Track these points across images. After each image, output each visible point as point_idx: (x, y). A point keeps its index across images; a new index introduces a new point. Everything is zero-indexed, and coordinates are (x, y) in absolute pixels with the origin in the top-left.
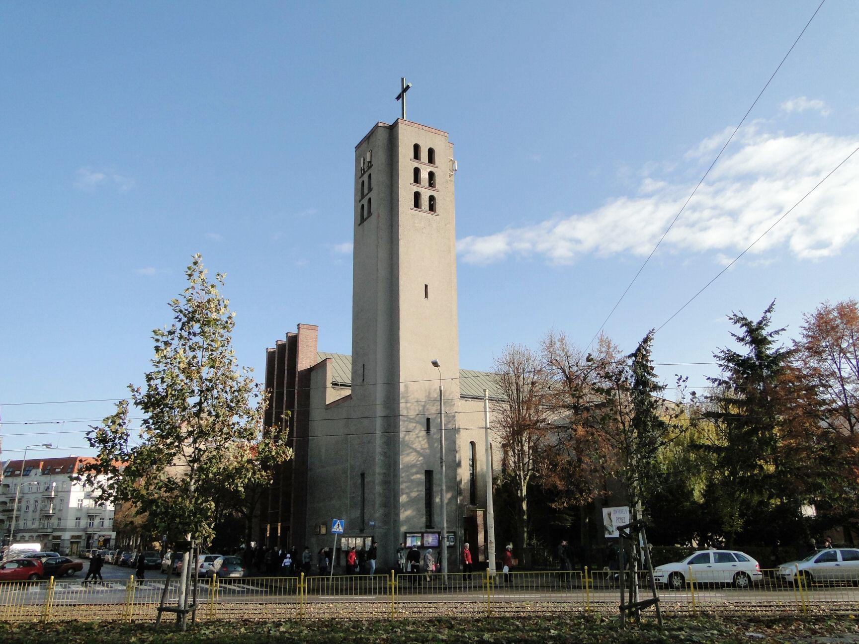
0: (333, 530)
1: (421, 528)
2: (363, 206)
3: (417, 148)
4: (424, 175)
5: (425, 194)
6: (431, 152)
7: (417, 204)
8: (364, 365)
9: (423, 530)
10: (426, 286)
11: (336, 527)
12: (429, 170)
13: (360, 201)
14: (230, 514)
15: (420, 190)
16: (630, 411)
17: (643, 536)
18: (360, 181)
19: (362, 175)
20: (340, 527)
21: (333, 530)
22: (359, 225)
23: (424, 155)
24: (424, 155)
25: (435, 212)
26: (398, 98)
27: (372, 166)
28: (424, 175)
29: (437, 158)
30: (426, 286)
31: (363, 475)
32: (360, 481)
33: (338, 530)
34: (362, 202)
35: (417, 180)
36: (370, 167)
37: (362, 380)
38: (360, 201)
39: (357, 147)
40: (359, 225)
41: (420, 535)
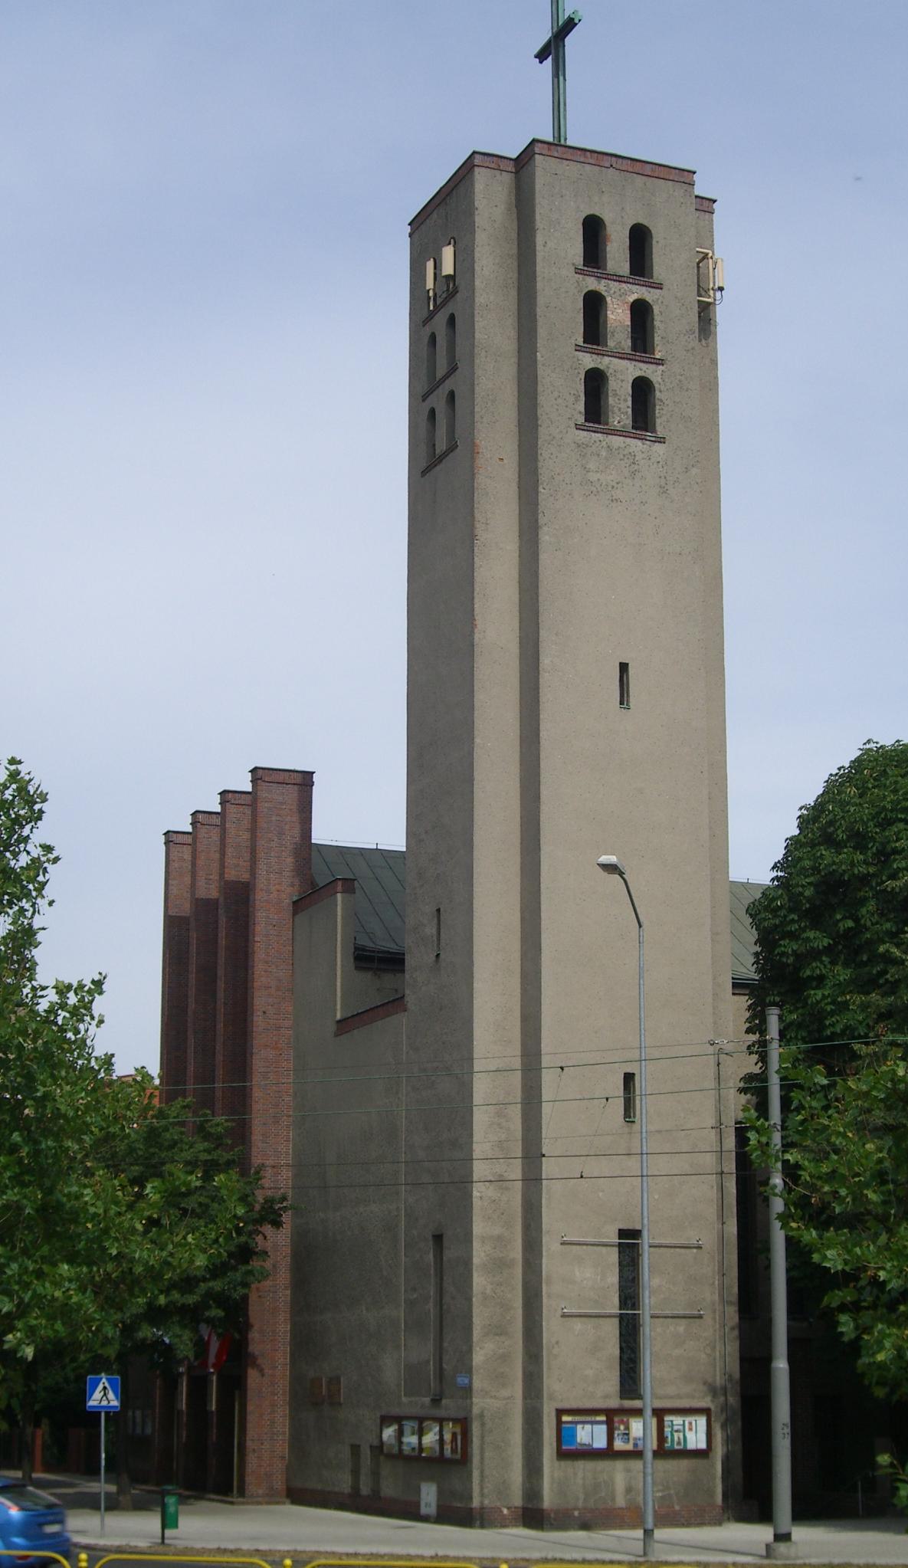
0: (91, 1403)
1: (606, 1397)
2: (432, 412)
3: (593, 229)
4: (618, 316)
5: (622, 374)
6: (640, 238)
7: (595, 411)
8: (438, 910)
9: (614, 1402)
10: (624, 668)
11: (98, 1394)
12: (632, 298)
13: (425, 398)
14: (158, 1331)
15: (604, 363)
16: (149, 1256)
17: (652, 1443)
18: (427, 331)
19: (432, 315)
20: (111, 1395)
21: (91, 1403)
22: (424, 473)
23: (617, 253)
24: (617, 253)
25: (654, 431)
26: (542, 56)
27: (456, 291)
28: (618, 316)
29: (660, 265)
30: (624, 668)
31: (438, 1239)
32: (431, 1256)
33: (104, 1403)
34: (432, 401)
35: (594, 330)
36: (451, 294)
37: (442, 956)
38: (425, 398)
39: (416, 224)
40: (424, 473)
41: (603, 1418)
